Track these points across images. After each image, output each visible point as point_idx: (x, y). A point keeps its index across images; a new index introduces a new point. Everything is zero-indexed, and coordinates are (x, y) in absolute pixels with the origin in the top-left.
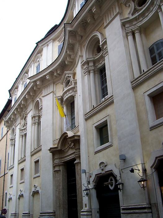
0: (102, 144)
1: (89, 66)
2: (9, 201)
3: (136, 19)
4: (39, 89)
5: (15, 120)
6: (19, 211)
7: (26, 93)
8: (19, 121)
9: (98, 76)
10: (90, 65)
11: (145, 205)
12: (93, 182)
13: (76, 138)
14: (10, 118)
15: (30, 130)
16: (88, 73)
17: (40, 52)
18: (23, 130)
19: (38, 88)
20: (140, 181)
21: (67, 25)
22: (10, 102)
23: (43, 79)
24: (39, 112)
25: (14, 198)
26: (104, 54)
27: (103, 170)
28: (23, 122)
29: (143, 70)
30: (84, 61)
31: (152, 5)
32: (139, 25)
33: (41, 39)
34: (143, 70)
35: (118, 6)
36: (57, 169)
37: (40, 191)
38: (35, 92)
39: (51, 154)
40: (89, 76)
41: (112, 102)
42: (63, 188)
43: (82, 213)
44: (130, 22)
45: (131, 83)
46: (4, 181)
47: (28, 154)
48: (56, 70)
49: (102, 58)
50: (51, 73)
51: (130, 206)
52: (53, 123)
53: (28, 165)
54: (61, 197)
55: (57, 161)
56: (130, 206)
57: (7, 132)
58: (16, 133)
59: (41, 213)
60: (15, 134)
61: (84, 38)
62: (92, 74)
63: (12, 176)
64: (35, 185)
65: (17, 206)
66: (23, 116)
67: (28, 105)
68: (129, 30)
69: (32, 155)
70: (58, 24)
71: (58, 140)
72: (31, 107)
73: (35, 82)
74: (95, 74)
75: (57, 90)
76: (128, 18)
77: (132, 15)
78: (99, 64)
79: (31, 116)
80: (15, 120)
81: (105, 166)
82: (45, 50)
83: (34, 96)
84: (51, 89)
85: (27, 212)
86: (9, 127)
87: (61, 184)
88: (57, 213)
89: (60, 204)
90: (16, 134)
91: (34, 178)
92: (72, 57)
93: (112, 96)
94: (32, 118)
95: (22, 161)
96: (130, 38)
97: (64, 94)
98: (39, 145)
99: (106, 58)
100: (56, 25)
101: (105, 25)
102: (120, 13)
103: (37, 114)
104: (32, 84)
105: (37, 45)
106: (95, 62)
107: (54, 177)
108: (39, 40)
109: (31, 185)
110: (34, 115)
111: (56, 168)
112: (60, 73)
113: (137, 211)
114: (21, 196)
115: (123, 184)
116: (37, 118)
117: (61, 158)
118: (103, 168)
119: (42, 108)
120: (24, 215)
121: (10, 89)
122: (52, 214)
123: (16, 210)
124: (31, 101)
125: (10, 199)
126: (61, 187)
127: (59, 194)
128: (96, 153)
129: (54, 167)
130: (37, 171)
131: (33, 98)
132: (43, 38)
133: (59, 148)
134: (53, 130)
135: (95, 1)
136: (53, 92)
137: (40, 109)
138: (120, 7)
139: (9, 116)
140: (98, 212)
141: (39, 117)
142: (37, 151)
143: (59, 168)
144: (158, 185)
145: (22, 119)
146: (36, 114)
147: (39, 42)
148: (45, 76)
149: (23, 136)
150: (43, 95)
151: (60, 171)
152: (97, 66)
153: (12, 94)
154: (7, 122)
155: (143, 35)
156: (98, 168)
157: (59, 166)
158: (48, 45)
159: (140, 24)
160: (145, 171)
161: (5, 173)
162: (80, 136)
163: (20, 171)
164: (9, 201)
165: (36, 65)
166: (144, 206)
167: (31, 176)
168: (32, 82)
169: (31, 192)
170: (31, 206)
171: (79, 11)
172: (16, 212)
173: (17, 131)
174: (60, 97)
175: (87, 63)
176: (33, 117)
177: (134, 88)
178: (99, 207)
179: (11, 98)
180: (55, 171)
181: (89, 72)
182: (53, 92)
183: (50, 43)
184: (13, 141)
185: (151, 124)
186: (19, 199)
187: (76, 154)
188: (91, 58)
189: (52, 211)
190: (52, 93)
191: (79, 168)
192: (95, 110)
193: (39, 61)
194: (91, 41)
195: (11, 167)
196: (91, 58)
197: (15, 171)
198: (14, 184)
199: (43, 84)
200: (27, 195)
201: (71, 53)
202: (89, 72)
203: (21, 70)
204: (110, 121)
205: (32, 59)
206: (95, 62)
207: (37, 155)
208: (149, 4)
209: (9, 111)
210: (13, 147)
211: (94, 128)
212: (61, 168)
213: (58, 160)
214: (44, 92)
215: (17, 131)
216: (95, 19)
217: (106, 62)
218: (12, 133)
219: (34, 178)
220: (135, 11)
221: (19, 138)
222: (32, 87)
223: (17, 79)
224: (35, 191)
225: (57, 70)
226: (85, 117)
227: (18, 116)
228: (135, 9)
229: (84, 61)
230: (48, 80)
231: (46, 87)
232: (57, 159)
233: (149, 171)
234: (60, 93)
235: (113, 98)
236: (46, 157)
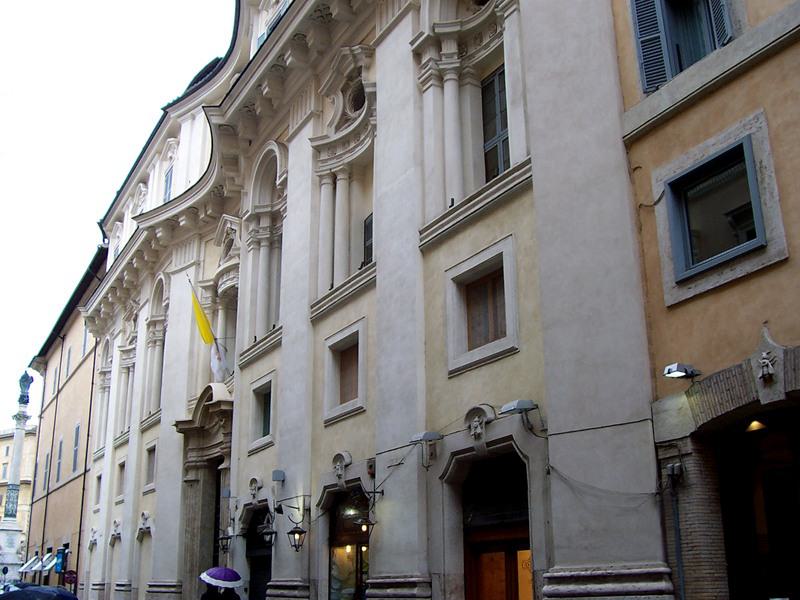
0: (472, 345)
1: (440, 56)
2: (91, 549)
3: (344, 141)
4: (165, 247)
5: (135, 287)
6: (110, 579)
7: (134, 253)
8: (120, 324)
9: (473, 96)
10: (444, 51)
11: (297, 580)
12: (240, 519)
13: (223, 407)
14: (98, 311)
15: (143, 356)
16: (436, 83)
17: (174, 133)
18: (158, 325)
19: (161, 246)
20: (293, 533)
21: (211, 111)
22: (102, 254)
23: (172, 224)
24: (272, 201)
25: (102, 543)
26: (503, 8)
27: (478, 437)
28: (130, 326)
29: (453, 200)
30: (422, 34)
31: (344, 144)
32: (346, 161)
33: (175, 99)
34: (453, 200)
35: (317, 94)
36: (191, 476)
37: (153, 530)
38: (156, 253)
39: (182, 435)
40: (439, 89)
41: (526, 187)
42: (203, 527)
43: (269, 592)
44: (331, 147)
45: (421, 233)
46: (84, 489)
47: (135, 427)
48: (203, 203)
49: (494, 24)
50: (193, 211)
51: (397, 577)
52: (191, 353)
53: (133, 454)
54: (197, 549)
55: (193, 456)
56: (397, 577)
57: (97, 343)
58: (168, 298)
59: (150, 586)
60: (164, 304)
61: (255, 146)
62: (450, 87)
63: (99, 478)
64: (143, 514)
65: (108, 563)
66: (131, 313)
67: (142, 285)
68: (326, 168)
69: (116, 448)
70: (222, 54)
71: (196, 402)
72: (147, 293)
73: (152, 228)
74: (461, 86)
75: (207, 260)
76: (326, 137)
77: (338, 129)
78: (479, 51)
79: (412, 43)
80: (111, 317)
81: (259, 488)
82: (186, 128)
83: (154, 263)
84: (191, 254)
85: (124, 581)
86: (99, 332)
87: (199, 517)
88: (186, 586)
89: (192, 565)
90: (168, 304)
91: (145, 493)
92: (237, 181)
93: (529, 161)
94: (149, 325)
95: (122, 443)
96: (326, 190)
97: (221, 275)
98: (274, 330)
99: (507, 23)
100: (217, 60)
101: (291, 131)
102: (317, 115)
103: (267, 206)
104: (145, 233)
105: (166, 114)
106: (464, 41)
107: (185, 496)
108: (171, 102)
109: (136, 511)
110: (258, 211)
111: (190, 473)
112: (215, 215)
113: (285, 592)
114: (116, 538)
115: (276, 533)
116: (265, 223)
117: (203, 449)
118: (479, 430)
119: (285, 183)
120: (118, 588)
121: (102, 218)
122: (173, 589)
123: (104, 573)
124: (147, 276)
125: (94, 544)
126: (198, 524)
127: (192, 540)
128: (252, 453)
129: (187, 470)
130: (150, 477)
131: (152, 268)
132: (180, 96)
133: (197, 425)
134: (191, 371)
135: (315, 3)
136: (197, 264)
137: (278, 182)
138: (321, 98)
139: (95, 304)
140: (246, 590)
141: (276, 217)
142: (150, 424)
143: (197, 475)
144: (327, 543)
145: (128, 319)
146: (158, 316)
147: (170, 106)
148: (177, 216)
149: (129, 368)
150: (173, 268)
151: (197, 481)
152: (473, 56)
153: (107, 233)
154: (91, 319)
155: (356, 186)
156: (330, 468)
157: (197, 468)
158: (194, 118)
159: (348, 158)
160: (307, 510)
161: (54, 485)
162: (232, 402)
163: (117, 468)
164: (91, 549)
165: (166, 165)
166: (295, 583)
167: (138, 486)
168: (144, 229)
169: (135, 531)
170: (135, 566)
171: (262, 46)
172: (103, 579)
173: (116, 353)
174: (212, 283)
175: (436, 41)
176: (152, 324)
177: (427, 249)
178: (249, 579)
179: (106, 240)
180: (185, 481)
181: (440, 79)
182: (197, 264)
183: (198, 112)
184: (159, 327)
185: (328, 414)
186: (113, 545)
187: (223, 446)
188: (264, 207)
189: (173, 581)
190: (194, 267)
191: (227, 483)
192: (361, 280)
193: (171, 158)
194: (266, 163)
195: (151, 420)
196: (264, 207)
197: (106, 468)
198: (104, 497)
199: (172, 237)
200: (128, 535)
201: (232, 174)
202: (259, 243)
203: (144, 143)
204: (276, 385)
205: (156, 146)
206: (464, 41)
207: (350, 314)
208: (360, 124)
209: (101, 280)
210: (158, 349)
211: (252, 392)
212: (201, 475)
213: (194, 454)
214: (177, 261)
215: (116, 353)
216: (351, 7)
217: (509, 37)
218: (154, 296)
219: (145, 493)
220: (345, 120)
221: (120, 373)
222: (147, 242)
223: (119, 193)
224: (255, 502)
225: (205, 207)
226: (312, 313)
227: (118, 307)
228: (344, 114)
229: (422, 34)
230: (186, 229)
231: (183, 245)
232: (192, 450)
233: (315, 512)
234: (211, 272)
235: (530, 170)
236: (171, 443)
